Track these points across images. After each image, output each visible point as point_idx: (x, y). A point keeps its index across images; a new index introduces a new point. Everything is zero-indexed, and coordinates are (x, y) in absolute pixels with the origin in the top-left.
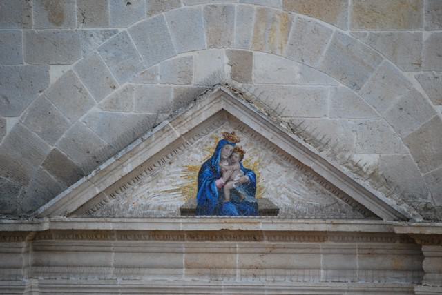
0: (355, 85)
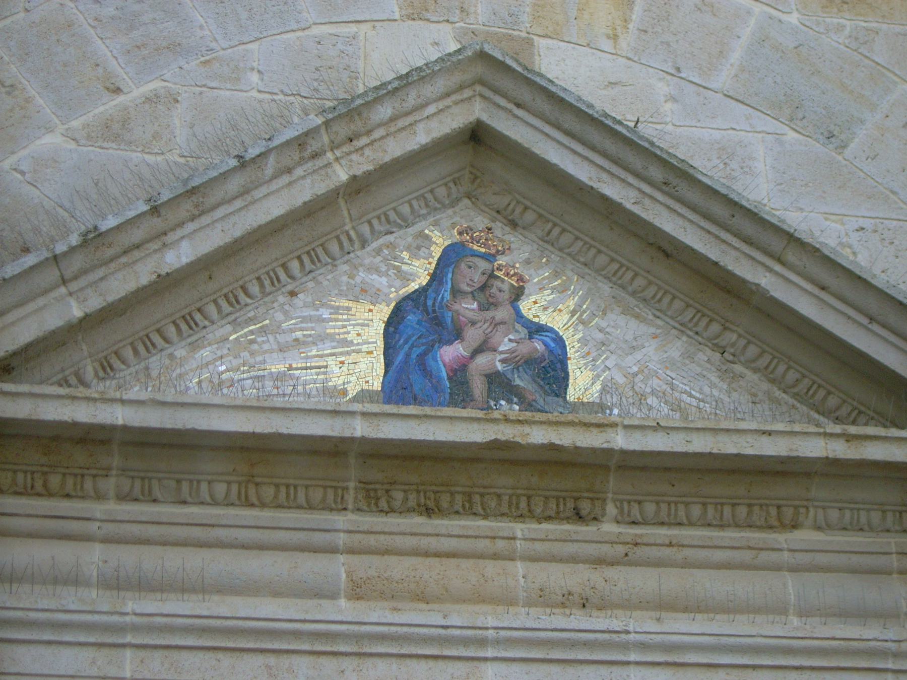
0: (831, 136)
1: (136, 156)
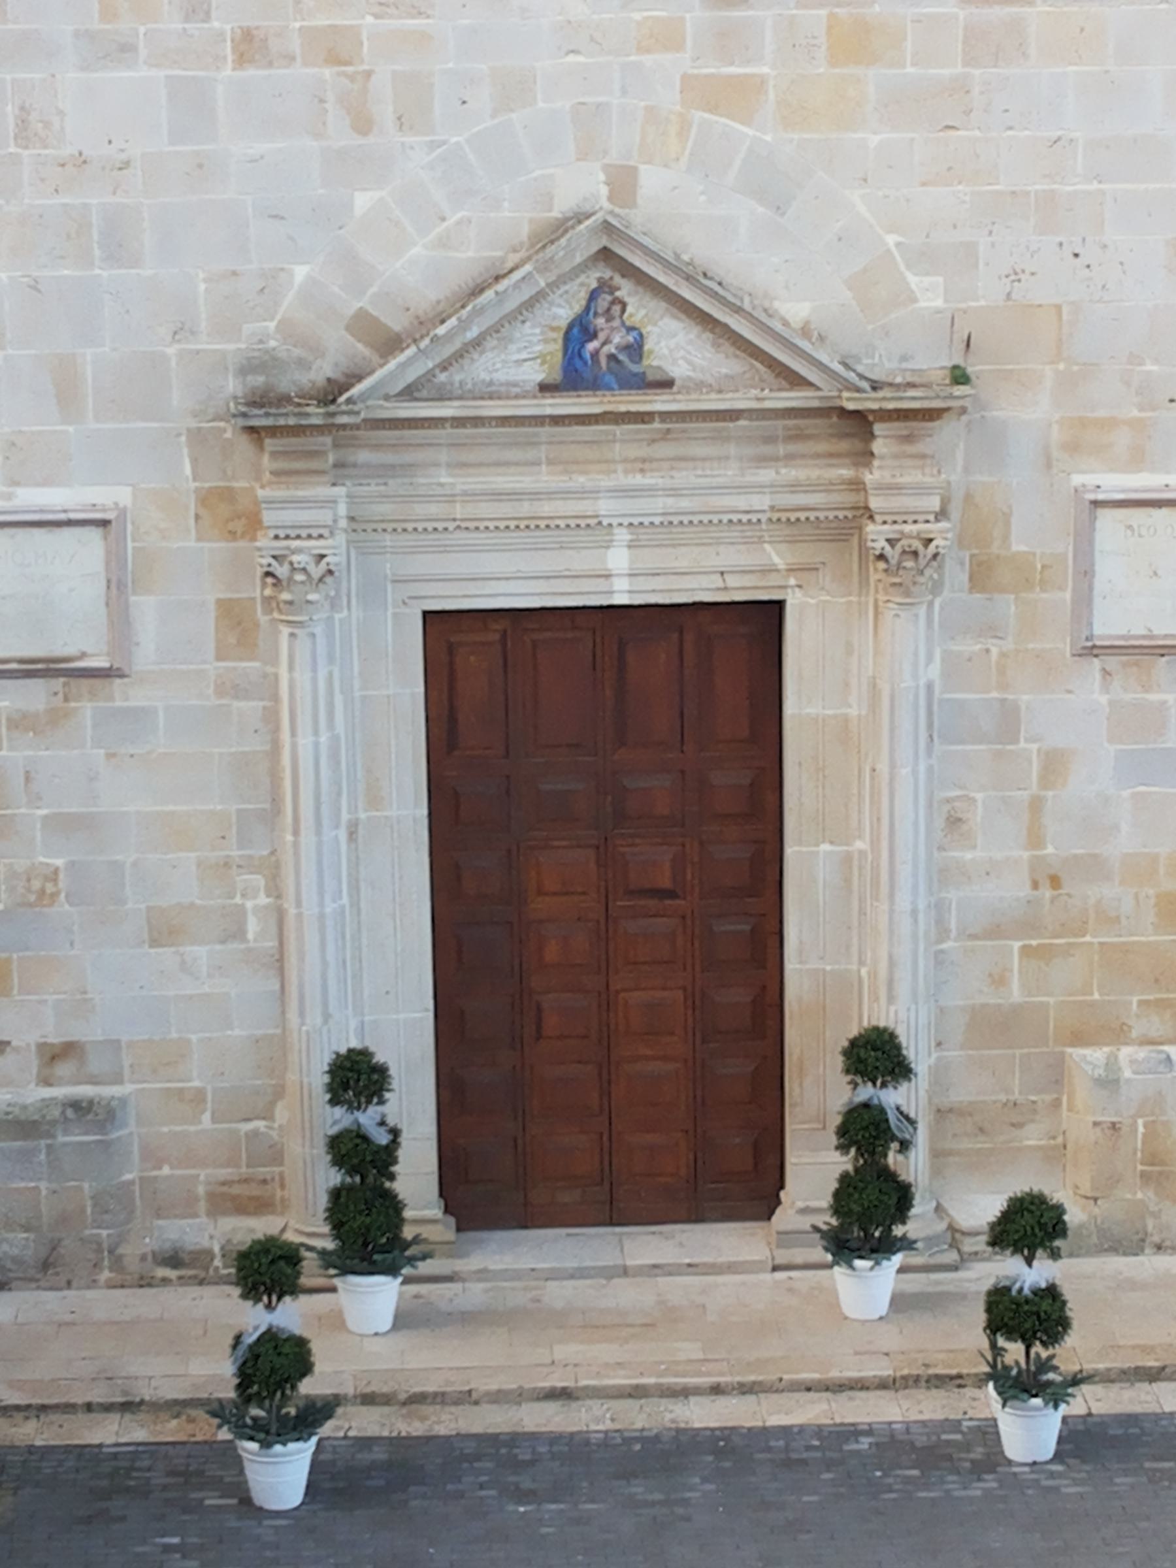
1: (10, 26)
